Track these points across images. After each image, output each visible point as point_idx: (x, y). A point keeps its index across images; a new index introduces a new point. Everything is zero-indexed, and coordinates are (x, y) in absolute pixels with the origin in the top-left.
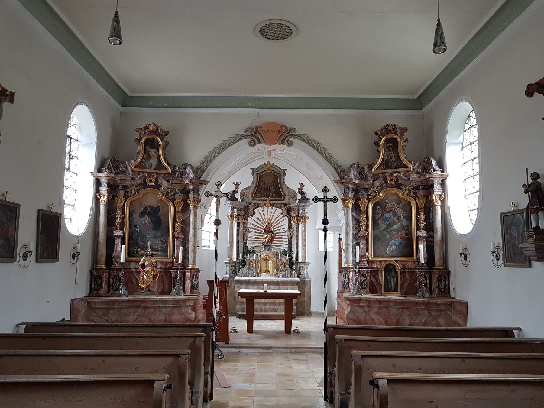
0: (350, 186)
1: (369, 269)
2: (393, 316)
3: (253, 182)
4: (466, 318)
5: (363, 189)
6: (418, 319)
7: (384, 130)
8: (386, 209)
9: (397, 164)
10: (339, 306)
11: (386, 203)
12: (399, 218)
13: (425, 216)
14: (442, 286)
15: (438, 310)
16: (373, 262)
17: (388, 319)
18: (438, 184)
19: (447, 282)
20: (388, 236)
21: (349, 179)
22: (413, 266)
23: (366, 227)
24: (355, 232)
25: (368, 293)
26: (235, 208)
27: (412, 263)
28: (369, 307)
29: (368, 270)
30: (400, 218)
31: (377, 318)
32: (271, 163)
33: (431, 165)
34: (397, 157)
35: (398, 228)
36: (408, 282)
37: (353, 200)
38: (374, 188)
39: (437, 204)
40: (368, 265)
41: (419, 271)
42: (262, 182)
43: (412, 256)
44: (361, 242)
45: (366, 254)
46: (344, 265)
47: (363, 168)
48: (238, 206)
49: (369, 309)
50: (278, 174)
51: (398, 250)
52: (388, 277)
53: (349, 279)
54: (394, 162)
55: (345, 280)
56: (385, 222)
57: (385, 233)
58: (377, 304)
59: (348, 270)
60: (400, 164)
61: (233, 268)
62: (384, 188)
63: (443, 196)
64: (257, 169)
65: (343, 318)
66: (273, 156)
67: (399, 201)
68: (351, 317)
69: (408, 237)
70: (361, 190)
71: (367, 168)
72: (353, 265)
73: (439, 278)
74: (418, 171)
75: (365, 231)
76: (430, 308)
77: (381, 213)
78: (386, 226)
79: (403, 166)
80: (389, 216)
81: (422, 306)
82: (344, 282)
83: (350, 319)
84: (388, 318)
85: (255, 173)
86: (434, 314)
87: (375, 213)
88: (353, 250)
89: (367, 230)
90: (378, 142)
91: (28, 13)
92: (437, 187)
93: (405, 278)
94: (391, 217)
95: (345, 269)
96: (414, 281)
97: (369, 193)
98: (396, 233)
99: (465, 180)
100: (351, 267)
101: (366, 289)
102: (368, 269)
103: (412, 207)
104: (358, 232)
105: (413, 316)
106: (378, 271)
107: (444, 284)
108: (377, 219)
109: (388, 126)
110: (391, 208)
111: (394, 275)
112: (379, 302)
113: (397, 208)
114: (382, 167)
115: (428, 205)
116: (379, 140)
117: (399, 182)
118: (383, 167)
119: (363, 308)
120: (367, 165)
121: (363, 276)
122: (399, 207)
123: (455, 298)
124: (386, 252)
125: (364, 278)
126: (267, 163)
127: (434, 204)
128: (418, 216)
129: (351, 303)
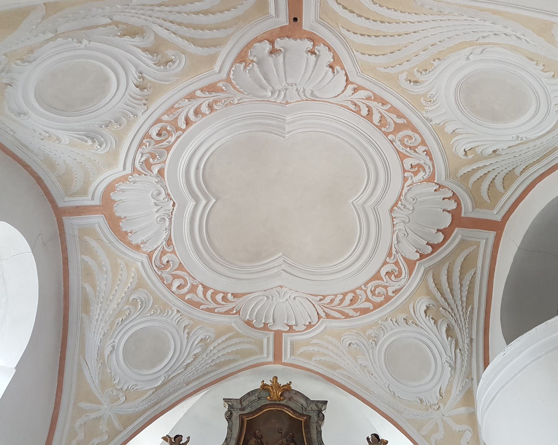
3: (226, 439)
32: (282, 382)
42: (254, 439)
50: (302, 415)
64: (241, 400)
66: (287, 358)
85: (236, 414)
91: (516, 249)
126: (269, 383)
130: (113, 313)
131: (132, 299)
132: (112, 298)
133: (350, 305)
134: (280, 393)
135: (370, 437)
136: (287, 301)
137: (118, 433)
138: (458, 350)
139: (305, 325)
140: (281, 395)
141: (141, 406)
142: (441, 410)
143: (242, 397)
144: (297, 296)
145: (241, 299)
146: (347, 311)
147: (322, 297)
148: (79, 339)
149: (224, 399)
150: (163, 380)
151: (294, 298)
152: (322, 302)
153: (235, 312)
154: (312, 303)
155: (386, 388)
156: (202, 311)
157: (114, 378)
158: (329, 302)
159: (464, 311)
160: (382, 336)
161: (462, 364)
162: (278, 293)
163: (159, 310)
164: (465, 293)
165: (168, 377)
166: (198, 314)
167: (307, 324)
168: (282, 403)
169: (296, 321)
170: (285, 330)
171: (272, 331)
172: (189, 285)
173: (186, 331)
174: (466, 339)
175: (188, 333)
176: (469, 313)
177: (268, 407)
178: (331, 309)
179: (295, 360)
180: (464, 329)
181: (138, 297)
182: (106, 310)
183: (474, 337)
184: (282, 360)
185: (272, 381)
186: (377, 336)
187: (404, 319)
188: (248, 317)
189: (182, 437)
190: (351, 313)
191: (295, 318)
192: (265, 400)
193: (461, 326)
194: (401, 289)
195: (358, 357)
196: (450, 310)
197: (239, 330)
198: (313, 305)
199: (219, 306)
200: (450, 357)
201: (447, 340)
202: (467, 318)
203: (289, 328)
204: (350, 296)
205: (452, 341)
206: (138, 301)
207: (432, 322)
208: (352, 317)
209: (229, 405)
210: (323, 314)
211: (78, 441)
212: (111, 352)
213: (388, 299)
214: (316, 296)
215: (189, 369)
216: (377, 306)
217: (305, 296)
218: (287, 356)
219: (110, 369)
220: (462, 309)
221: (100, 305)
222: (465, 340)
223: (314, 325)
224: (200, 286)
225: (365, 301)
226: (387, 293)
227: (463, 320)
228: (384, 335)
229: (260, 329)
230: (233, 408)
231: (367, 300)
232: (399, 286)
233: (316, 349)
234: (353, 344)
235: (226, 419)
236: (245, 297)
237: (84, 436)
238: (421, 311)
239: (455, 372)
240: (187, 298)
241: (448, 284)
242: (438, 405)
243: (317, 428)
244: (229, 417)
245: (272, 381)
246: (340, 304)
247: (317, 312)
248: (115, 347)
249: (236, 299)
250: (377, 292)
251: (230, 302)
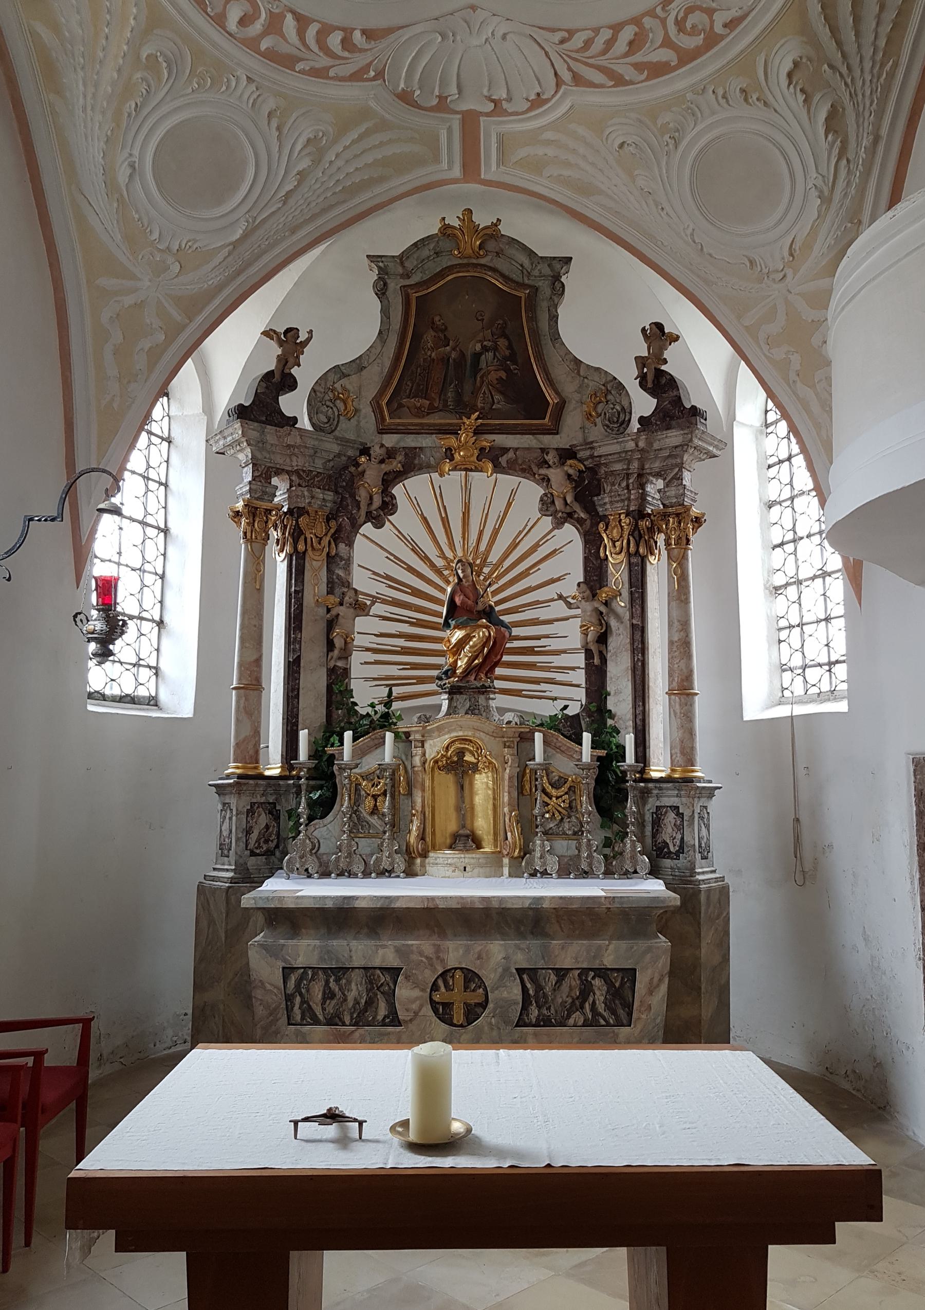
3: (380, 332)
26: (278, 472)
32: (482, 219)
48: (297, 463)
50: (521, 285)
61: (263, 819)
64: (402, 258)
66: (491, 169)
85: (394, 285)
126: (456, 223)
130: (113, 91)
131: (145, 56)
132: (101, 55)
133: (626, 55)
134: (478, 243)
135: (648, 327)
136: (487, 44)
137: (183, 328)
138: (844, 162)
139: (527, 99)
140: (480, 247)
141: (212, 278)
142: (787, 281)
143: (403, 252)
144: (510, 30)
145: (382, 44)
146: (620, 69)
147: (566, 35)
148: (58, 152)
149: (367, 256)
150: (244, 228)
151: (504, 37)
152: (565, 46)
153: (372, 74)
154: (543, 49)
155: (686, 235)
156: (300, 75)
157: (149, 229)
158: (582, 48)
159: (875, 71)
160: (692, 126)
161: (846, 193)
162: (465, 25)
163: (209, 79)
164: (886, 28)
165: (254, 222)
166: (292, 81)
167: (533, 97)
168: (482, 263)
169: (508, 90)
170: (486, 111)
171: (457, 113)
172: (263, 15)
173: (274, 123)
174: (865, 138)
175: (278, 128)
176: (884, 75)
177: (455, 270)
178: (586, 64)
179: (507, 174)
180: (867, 114)
181: (157, 51)
182: (96, 86)
183: (884, 132)
184: (480, 175)
185: (461, 217)
186: (679, 128)
187: (743, 91)
188: (402, 85)
189: (298, 330)
190: (628, 73)
191: (507, 84)
192: (447, 257)
193: (861, 109)
194: (747, 15)
195: (636, 173)
196: (844, 70)
197: (384, 113)
198: (547, 54)
199: (338, 62)
200: (823, 177)
201: (824, 139)
202: (879, 90)
203: (493, 104)
204: (628, 33)
205: (834, 142)
206: (160, 59)
207: (801, 98)
208: (631, 83)
209: (379, 268)
210: (566, 76)
211: (115, 345)
212: (131, 176)
213: (712, 40)
214: (553, 30)
215: (292, 202)
216: (686, 57)
217: (528, 30)
218: (490, 168)
219: (137, 212)
220: (873, 67)
221: (81, 74)
222: (862, 139)
223: (547, 101)
224: (289, 16)
225: (662, 46)
226: (712, 27)
227: (869, 93)
228: (695, 124)
229: (431, 109)
230: (387, 274)
231: (667, 43)
232: (740, 11)
233: (551, 152)
234: (628, 145)
235: (376, 294)
236: (392, 37)
237: (122, 337)
238: (781, 68)
239: (828, 209)
240: (264, 45)
241: (852, 7)
242: (783, 272)
243: (549, 310)
244: (381, 291)
245: (461, 217)
246: (605, 52)
247: (554, 69)
248: (137, 165)
249: (373, 42)
250: (688, 25)
251: (361, 51)
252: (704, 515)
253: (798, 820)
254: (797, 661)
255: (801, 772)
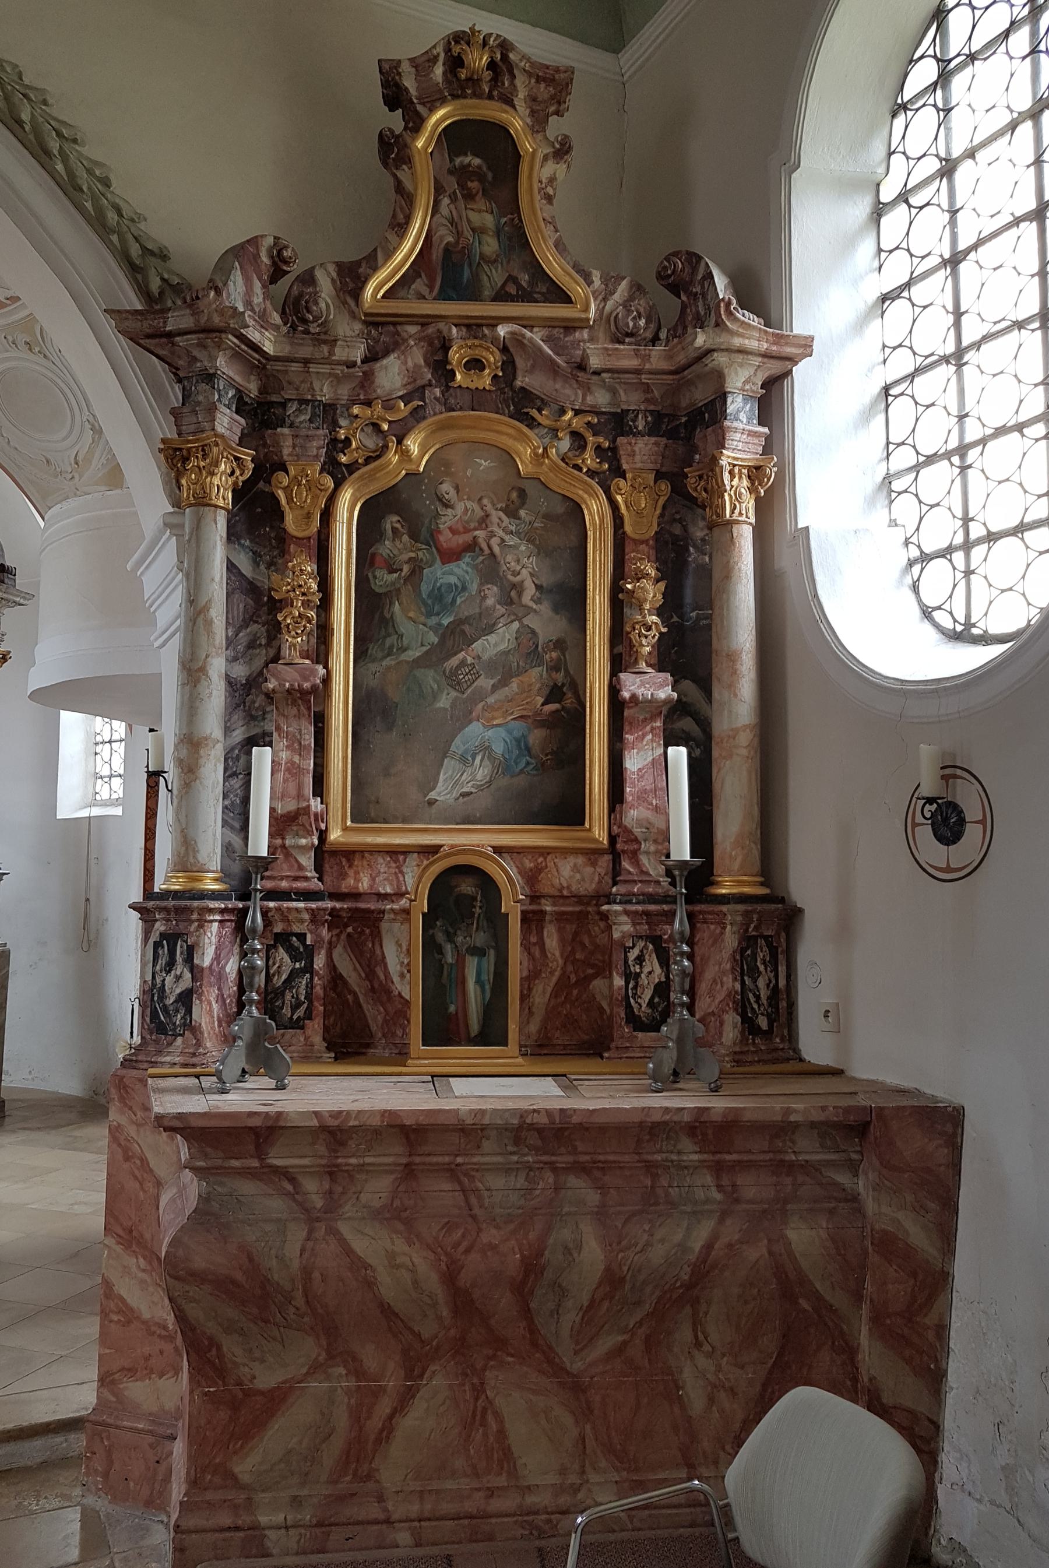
0: (223, 364)
1: (329, 904)
2: (498, 1227)
4: (949, 1205)
5: (303, 402)
6: (662, 1241)
7: (439, 71)
8: (442, 538)
9: (512, 279)
10: (119, 1156)
11: (440, 500)
12: (511, 594)
13: (662, 585)
14: (758, 998)
15: (783, 1167)
16: (349, 854)
17: (467, 1251)
18: (745, 404)
19: (782, 969)
20: (444, 702)
21: (221, 312)
22: (583, 880)
23: (313, 640)
24: (240, 671)
25: (318, 1060)
27: (580, 860)
28: (332, 1173)
29: (319, 909)
30: (520, 594)
31: (391, 1256)
33: (704, 295)
34: (510, 239)
35: (506, 653)
36: (554, 979)
37: (237, 459)
38: (368, 403)
39: (741, 514)
40: (320, 879)
41: (629, 907)
43: (583, 824)
44: (278, 728)
45: (313, 809)
46: (167, 879)
47: (308, 278)
49: (331, 1192)
51: (504, 781)
52: (448, 948)
53: (196, 972)
54: (496, 261)
55: (169, 980)
56: (429, 614)
57: (429, 677)
58: (393, 1154)
59: (191, 910)
60: (524, 279)
62: (429, 410)
63: (772, 471)
65: (148, 1236)
67: (514, 495)
68: (199, 1263)
69: (563, 708)
70: (292, 408)
71: (333, 281)
72: (225, 875)
73: (743, 951)
74: (627, 324)
75: (307, 661)
76: (735, 1157)
77: (410, 559)
78: (436, 640)
79: (544, 290)
80: (453, 580)
81: (686, 1143)
82: (163, 988)
83: (198, 1277)
84: (465, 1244)
86: (750, 1193)
87: (374, 555)
88: (226, 779)
89: (321, 652)
90: (400, 136)
92: (743, 416)
93: (537, 954)
94: (464, 589)
95: (171, 903)
96: (590, 971)
97: (342, 434)
98: (492, 682)
99: (886, 389)
100: (213, 891)
101: (302, 1028)
102: (320, 904)
103: (590, 534)
104: (266, 665)
105: (627, 1221)
106: (383, 912)
107: (768, 985)
108: (385, 594)
109: (468, 44)
110: (467, 530)
111: (480, 939)
112: (408, 1138)
113: (501, 533)
114: (419, 285)
115: (677, 530)
116: (406, 128)
117: (518, 383)
118: (431, 288)
119: (289, 1187)
120: (332, 268)
121: (290, 950)
122: (513, 528)
123: (837, 1073)
124: (432, 795)
125: (294, 959)
127: (721, 514)
128: (629, 586)
129: (206, 1156)
252: (9, 652)
253: (87, 900)
254: (106, 772)
255: (92, 862)
